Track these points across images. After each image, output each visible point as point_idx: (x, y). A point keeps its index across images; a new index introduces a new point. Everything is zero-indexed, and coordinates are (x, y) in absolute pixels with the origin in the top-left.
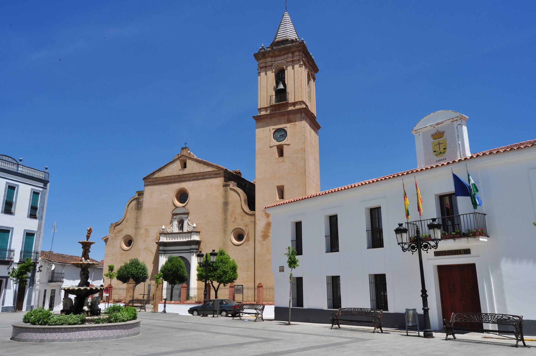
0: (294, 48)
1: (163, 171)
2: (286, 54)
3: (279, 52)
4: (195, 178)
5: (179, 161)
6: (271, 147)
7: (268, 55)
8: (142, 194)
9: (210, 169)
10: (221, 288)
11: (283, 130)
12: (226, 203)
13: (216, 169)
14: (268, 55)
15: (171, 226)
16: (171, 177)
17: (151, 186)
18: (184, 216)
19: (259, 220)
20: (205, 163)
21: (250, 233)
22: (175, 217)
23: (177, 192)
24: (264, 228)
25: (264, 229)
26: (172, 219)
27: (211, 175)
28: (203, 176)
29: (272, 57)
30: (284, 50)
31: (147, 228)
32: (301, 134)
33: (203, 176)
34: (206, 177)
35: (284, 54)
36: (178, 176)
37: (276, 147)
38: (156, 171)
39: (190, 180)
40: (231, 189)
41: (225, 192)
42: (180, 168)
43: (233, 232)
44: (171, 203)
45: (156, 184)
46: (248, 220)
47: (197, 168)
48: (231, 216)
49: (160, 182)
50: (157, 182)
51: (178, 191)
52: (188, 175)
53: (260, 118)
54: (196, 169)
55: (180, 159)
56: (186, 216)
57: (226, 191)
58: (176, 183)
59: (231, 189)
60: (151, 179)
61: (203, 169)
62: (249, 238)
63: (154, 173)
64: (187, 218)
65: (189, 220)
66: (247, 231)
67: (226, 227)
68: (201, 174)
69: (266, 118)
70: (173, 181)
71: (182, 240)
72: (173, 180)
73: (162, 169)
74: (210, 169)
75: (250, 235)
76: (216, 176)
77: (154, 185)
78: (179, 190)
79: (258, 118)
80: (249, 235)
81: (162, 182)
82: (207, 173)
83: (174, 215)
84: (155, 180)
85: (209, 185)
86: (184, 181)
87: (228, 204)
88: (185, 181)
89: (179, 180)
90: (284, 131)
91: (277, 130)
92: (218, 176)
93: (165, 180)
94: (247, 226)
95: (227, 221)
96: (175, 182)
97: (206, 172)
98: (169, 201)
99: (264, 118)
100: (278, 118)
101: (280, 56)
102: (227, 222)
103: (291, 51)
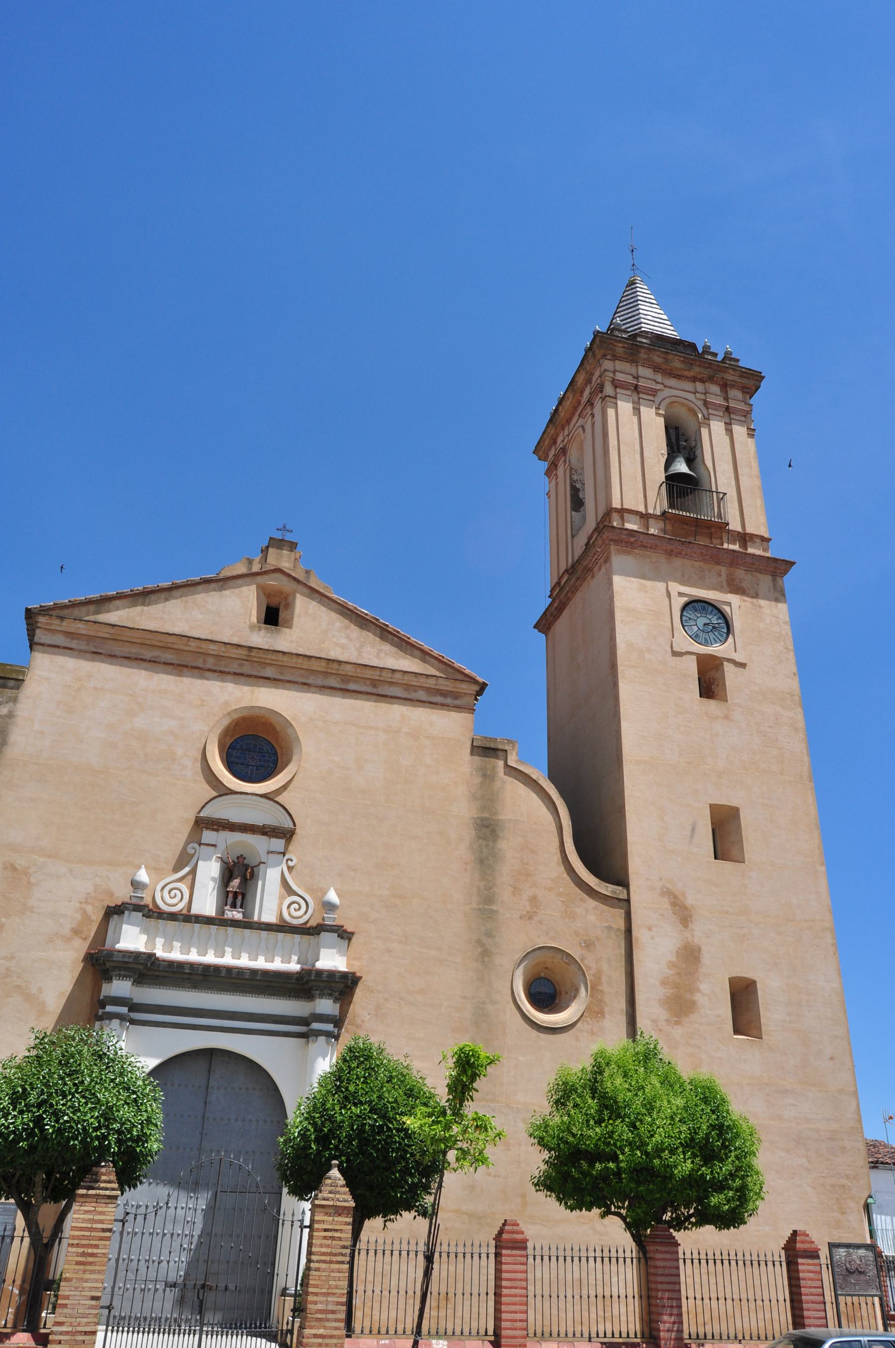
0: (732, 373)
1: (160, 606)
2: (702, 381)
3: (683, 362)
4: (333, 682)
5: (254, 586)
6: (675, 654)
7: (646, 356)
8: (11, 683)
9: (407, 664)
10: (688, 1256)
11: (715, 611)
12: (487, 827)
13: (438, 670)
14: (646, 356)
15: (180, 880)
16: (204, 645)
17: (77, 657)
18: (258, 844)
19: (650, 929)
20: (385, 633)
21: (604, 979)
22: (208, 836)
23: (232, 721)
24: (671, 965)
25: (671, 972)
26: (187, 843)
27: (416, 691)
28: (374, 686)
29: (657, 369)
30: (699, 366)
31: (20, 862)
32: (782, 643)
33: (374, 683)
34: (392, 694)
35: (694, 379)
36: (244, 652)
37: (694, 657)
38: (120, 597)
39: (306, 686)
40: (512, 771)
41: (484, 775)
42: (254, 619)
43: (523, 965)
44: (192, 768)
45: (111, 657)
46: (592, 918)
47: (344, 641)
48: (516, 891)
49: (134, 650)
50: (118, 649)
51: (235, 716)
52: (300, 660)
53: (632, 539)
54: (343, 647)
55: (260, 579)
56: (278, 844)
57: (487, 776)
58: (229, 677)
59: (512, 771)
60: (81, 625)
61: (378, 656)
62: (601, 1001)
63: (103, 602)
64: (284, 854)
65: (290, 869)
66: (593, 971)
67: (489, 934)
68: (369, 674)
69: (651, 548)
70: (208, 666)
71: (244, 961)
72: (210, 663)
73: (153, 597)
74: (407, 664)
75: (605, 987)
76: (438, 699)
77: (96, 654)
78: (245, 713)
79: (623, 537)
80: (600, 988)
81: (149, 654)
82: (398, 676)
83: (202, 824)
84: (105, 632)
85: (405, 730)
86: (275, 680)
87: (501, 834)
88: (279, 680)
89: (247, 669)
90: (719, 615)
91: (693, 605)
92: (449, 701)
93: (165, 648)
94: (589, 945)
95: (494, 908)
96: (222, 674)
97: (393, 671)
98: (180, 751)
99: (645, 547)
100: (697, 564)
101: (678, 377)
102: (493, 911)
103: (723, 378)
